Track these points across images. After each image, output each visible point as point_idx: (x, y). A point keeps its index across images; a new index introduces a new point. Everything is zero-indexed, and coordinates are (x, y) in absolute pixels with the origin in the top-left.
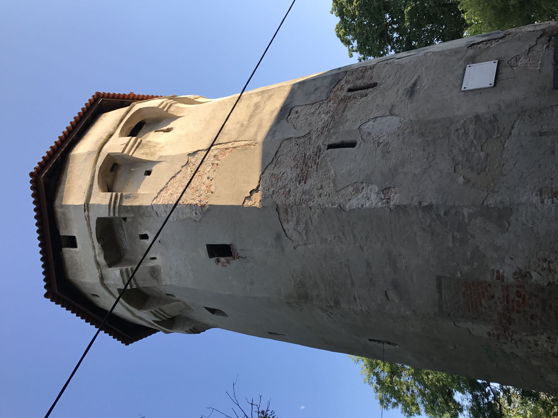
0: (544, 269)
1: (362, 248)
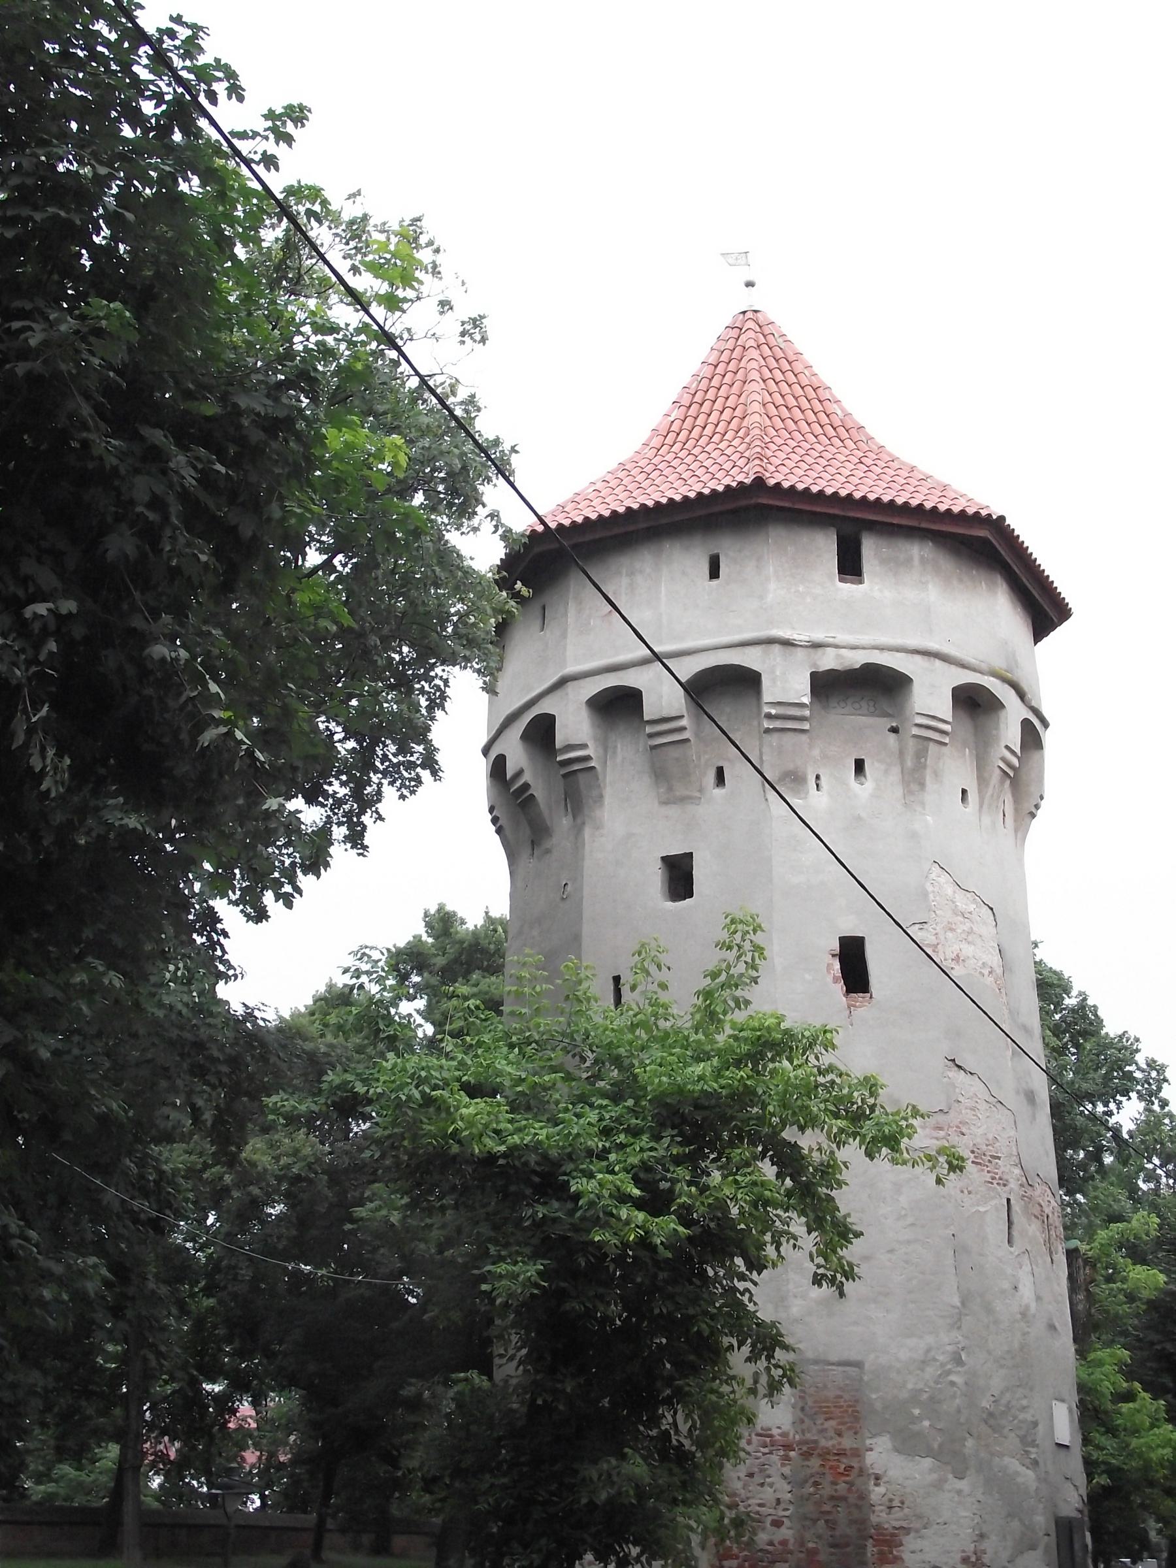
0: (891, 1500)
1: (891, 1251)
